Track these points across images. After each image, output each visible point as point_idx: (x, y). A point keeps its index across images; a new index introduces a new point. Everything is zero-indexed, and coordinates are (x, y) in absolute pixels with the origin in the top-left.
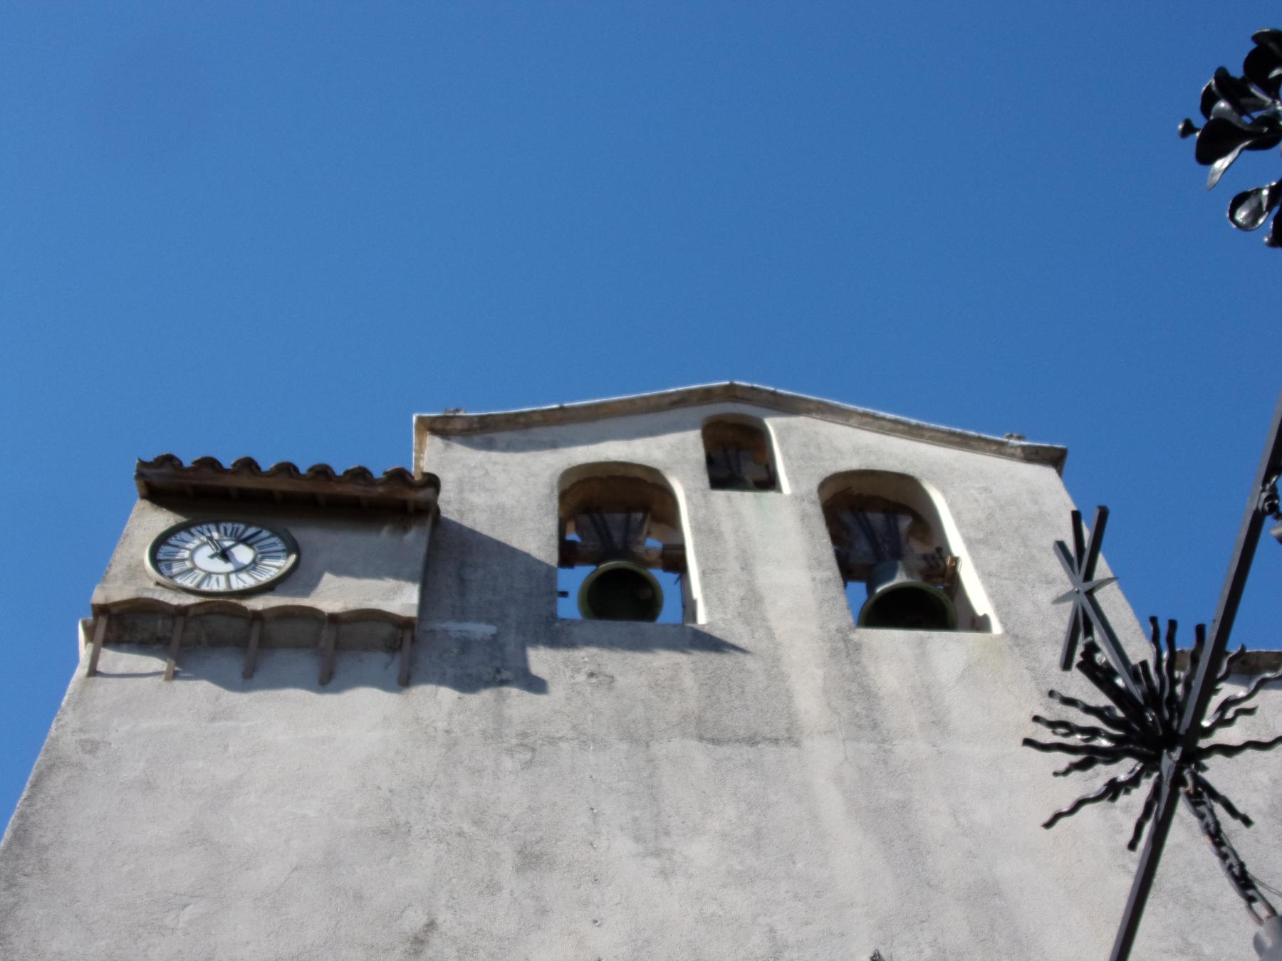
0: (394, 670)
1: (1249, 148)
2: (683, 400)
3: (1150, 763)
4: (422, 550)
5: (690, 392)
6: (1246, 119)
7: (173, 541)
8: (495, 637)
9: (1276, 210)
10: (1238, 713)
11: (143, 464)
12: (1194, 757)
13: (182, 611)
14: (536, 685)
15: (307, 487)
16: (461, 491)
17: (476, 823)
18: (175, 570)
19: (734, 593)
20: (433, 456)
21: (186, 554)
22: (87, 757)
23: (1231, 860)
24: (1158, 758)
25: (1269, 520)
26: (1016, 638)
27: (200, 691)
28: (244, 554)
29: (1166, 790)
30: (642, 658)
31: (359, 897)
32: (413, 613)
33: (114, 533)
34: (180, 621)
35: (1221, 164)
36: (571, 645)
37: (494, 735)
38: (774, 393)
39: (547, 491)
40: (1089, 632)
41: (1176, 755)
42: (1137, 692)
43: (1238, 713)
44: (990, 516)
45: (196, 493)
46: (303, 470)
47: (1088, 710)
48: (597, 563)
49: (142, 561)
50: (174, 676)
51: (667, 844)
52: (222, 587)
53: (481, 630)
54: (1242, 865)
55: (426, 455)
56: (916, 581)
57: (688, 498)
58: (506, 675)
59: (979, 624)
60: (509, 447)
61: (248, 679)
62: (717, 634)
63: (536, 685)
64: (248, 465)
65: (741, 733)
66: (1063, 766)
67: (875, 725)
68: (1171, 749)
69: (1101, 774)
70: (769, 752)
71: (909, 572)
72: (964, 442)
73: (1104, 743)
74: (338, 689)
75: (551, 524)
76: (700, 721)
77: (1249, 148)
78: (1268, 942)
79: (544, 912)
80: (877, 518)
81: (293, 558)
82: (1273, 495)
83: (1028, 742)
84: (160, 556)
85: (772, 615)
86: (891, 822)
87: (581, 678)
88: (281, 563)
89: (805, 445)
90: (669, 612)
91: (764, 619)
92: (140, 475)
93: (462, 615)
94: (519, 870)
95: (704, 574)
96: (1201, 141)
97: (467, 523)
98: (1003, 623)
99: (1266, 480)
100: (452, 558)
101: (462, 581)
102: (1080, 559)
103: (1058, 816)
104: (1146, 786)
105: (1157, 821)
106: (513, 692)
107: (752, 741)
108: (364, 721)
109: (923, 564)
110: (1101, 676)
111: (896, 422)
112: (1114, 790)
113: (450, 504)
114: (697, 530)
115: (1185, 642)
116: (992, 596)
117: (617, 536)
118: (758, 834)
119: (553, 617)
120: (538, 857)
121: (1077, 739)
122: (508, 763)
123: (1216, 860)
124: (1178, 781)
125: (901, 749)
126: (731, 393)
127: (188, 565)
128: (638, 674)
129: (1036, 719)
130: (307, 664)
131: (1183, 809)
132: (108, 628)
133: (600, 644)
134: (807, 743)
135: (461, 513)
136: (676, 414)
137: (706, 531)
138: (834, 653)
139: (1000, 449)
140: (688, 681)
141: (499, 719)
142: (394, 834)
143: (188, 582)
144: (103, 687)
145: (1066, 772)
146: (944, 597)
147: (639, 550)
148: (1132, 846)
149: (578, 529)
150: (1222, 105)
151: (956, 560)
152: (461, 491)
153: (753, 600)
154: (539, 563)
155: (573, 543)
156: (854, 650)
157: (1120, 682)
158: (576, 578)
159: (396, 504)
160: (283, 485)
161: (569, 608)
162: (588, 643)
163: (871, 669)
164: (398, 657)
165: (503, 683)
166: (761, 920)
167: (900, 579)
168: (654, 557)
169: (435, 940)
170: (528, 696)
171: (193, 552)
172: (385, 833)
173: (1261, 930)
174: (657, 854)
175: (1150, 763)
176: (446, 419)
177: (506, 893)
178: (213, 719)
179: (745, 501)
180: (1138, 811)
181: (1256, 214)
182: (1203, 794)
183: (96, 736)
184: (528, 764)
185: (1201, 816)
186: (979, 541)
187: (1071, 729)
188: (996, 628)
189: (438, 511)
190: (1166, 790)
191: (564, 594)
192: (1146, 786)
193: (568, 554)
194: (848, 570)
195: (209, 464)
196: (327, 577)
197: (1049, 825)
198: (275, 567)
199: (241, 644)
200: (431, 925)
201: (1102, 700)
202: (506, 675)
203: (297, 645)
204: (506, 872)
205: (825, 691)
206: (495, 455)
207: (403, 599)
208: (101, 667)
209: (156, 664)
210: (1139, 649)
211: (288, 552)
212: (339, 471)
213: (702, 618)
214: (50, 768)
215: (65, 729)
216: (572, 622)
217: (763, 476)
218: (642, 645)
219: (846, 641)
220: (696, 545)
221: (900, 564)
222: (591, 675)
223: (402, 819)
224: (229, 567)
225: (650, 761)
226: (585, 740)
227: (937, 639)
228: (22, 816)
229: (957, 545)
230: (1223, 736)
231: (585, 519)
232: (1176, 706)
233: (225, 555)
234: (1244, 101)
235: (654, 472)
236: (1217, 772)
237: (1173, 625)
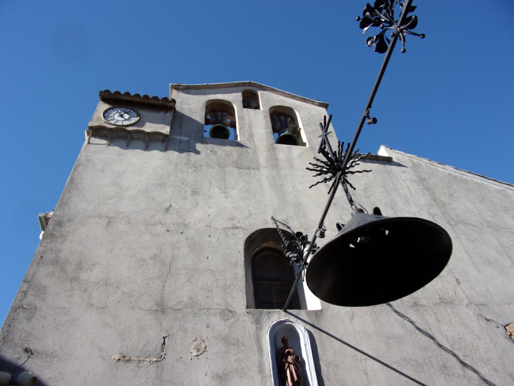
0: (163, 147)
1: (372, 25)
2: (238, 85)
3: (334, 175)
4: (171, 118)
5: (240, 83)
6: (373, 18)
7: (109, 112)
8: (188, 140)
9: (378, 41)
10: (356, 164)
11: (101, 92)
12: (344, 173)
13: (111, 129)
14: (198, 153)
15: (142, 100)
16: (181, 104)
17: (182, 183)
18: (109, 119)
19: (247, 134)
20: (174, 95)
21: (112, 115)
22: (88, 163)
23: (349, 196)
24: (336, 173)
25: (367, 119)
26: (311, 148)
27: (115, 149)
28: (126, 116)
29: (337, 181)
30: (224, 148)
31: (153, 199)
32: (168, 133)
33: (94, 109)
34: (110, 132)
35: (366, 29)
36: (207, 143)
37: (187, 164)
38: (260, 85)
39: (202, 105)
40: (325, 144)
41: (340, 173)
42: (333, 158)
43: (356, 164)
44: (309, 119)
45: (115, 100)
46: (142, 96)
47: (322, 162)
48: (214, 124)
49: (101, 117)
50: (109, 145)
51: (227, 191)
52: (121, 124)
53: (185, 139)
54: (351, 198)
55: (173, 94)
56: (290, 133)
57: (237, 110)
58: (190, 150)
59: (304, 144)
60: (194, 94)
61: (127, 146)
62: (242, 143)
63: (198, 153)
64: (128, 94)
65: (246, 167)
66: (315, 175)
67: (277, 166)
68: (339, 171)
69: (324, 176)
70: (252, 171)
71: (289, 131)
72: (305, 101)
73: (325, 170)
74: (149, 150)
75: (203, 114)
76: (236, 163)
77: (372, 25)
78: (354, 214)
79: (197, 204)
80: (283, 118)
81: (139, 118)
82: (368, 113)
83: (307, 168)
84: (106, 115)
85: (255, 139)
86: (279, 189)
87: (209, 151)
88: (136, 119)
89: (267, 99)
90: (231, 137)
91: (254, 140)
92: (100, 95)
93: (180, 135)
94: (192, 195)
95: (240, 129)
96: (361, 22)
97: (182, 112)
98: (309, 145)
99: (367, 109)
100: (178, 120)
101: (181, 126)
102: (325, 127)
103: (312, 186)
104: (333, 179)
105: (335, 187)
106: (192, 154)
107: (248, 169)
108: (155, 158)
109: (292, 130)
110: (326, 154)
111: (289, 94)
112: (326, 180)
113: (178, 107)
114: (239, 118)
115: (345, 147)
116: (307, 138)
117: (219, 118)
118: (248, 189)
119: (203, 137)
120: (197, 192)
121: (319, 169)
122: (190, 170)
123: (346, 196)
124: (340, 179)
125: (283, 172)
126: (250, 84)
127: (113, 118)
128: (224, 151)
129: (310, 163)
130: (142, 144)
131: (340, 185)
132: (93, 132)
133: (213, 144)
134: (261, 170)
135: (181, 110)
136: (235, 89)
137: (241, 118)
138: (269, 149)
139: (313, 103)
140: (234, 154)
141: (189, 160)
142: (162, 185)
143: (113, 122)
144: (91, 147)
145: (315, 176)
146: (296, 137)
147: (225, 122)
148: (329, 193)
149: (210, 116)
150: (368, 13)
151: (300, 129)
152: (181, 104)
153: (251, 136)
154: (200, 123)
155: (209, 119)
156: (274, 149)
157: (330, 156)
158: (209, 128)
159: (164, 106)
160: (136, 99)
161: (207, 135)
162: (211, 143)
163: (278, 153)
164: (164, 144)
165: (190, 151)
166: (248, 208)
167: (287, 133)
168: (228, 124)
169: (171, 209)
170: (196, 155)
171: (114, 115)
172: (160, 185)
173: (353, 211)
174: (225, 193)
175: (334, 175)
176: (178, 86)
177: (188, 199)
178: (119, 156)
179: (251, 111)
180: (330, 186)
181: (372, 43)
182: (345, 182)
183: (90, 158)
184: (195, 171)
185: (344, 187)
186: (307, 125)
187: (318, 166)
188: (308, 145)
189: (175, 109)
190: (337, 181)
191: (206, 131)
192: (333, 179)
193: (207, 122)
194: (274, 130)
195: (118, 93)
196: (147, 123)
197: (310, 187)
198: (134, 120)
199: (126, 138)
200: (170, 206)
201: (325, 159)
202: (190, 150)
203: (139, 139)
204: (188, 195)
205: (266, 158)
206: (190, 96)
207: (166, 130)
208: (91, 142)
209: (105, 142)
210: (335, 148)
211: (138, 116)
212: (151, 97)
213: (239, 139)
214: (78, 165)
215: (82, 156)
216: (207, 138)
217: (256, 106)
218: (224, 145)
219: (272, 146)
220: (238, 122)
221: (287, 129)
222: (211, 151)
223: (164, 182)
224: (123, 119)
225: (224, 172)
226: (209, 166)
227: (294, 147)
228: (72, 176)
229: (301, 125)
230: (351, 169)
231: (212, 113)
232: (342, 162)
233: (122, 116)
234: (373, 13)
235: (229, 103)
236: (350, 178)
237: (343, 143)
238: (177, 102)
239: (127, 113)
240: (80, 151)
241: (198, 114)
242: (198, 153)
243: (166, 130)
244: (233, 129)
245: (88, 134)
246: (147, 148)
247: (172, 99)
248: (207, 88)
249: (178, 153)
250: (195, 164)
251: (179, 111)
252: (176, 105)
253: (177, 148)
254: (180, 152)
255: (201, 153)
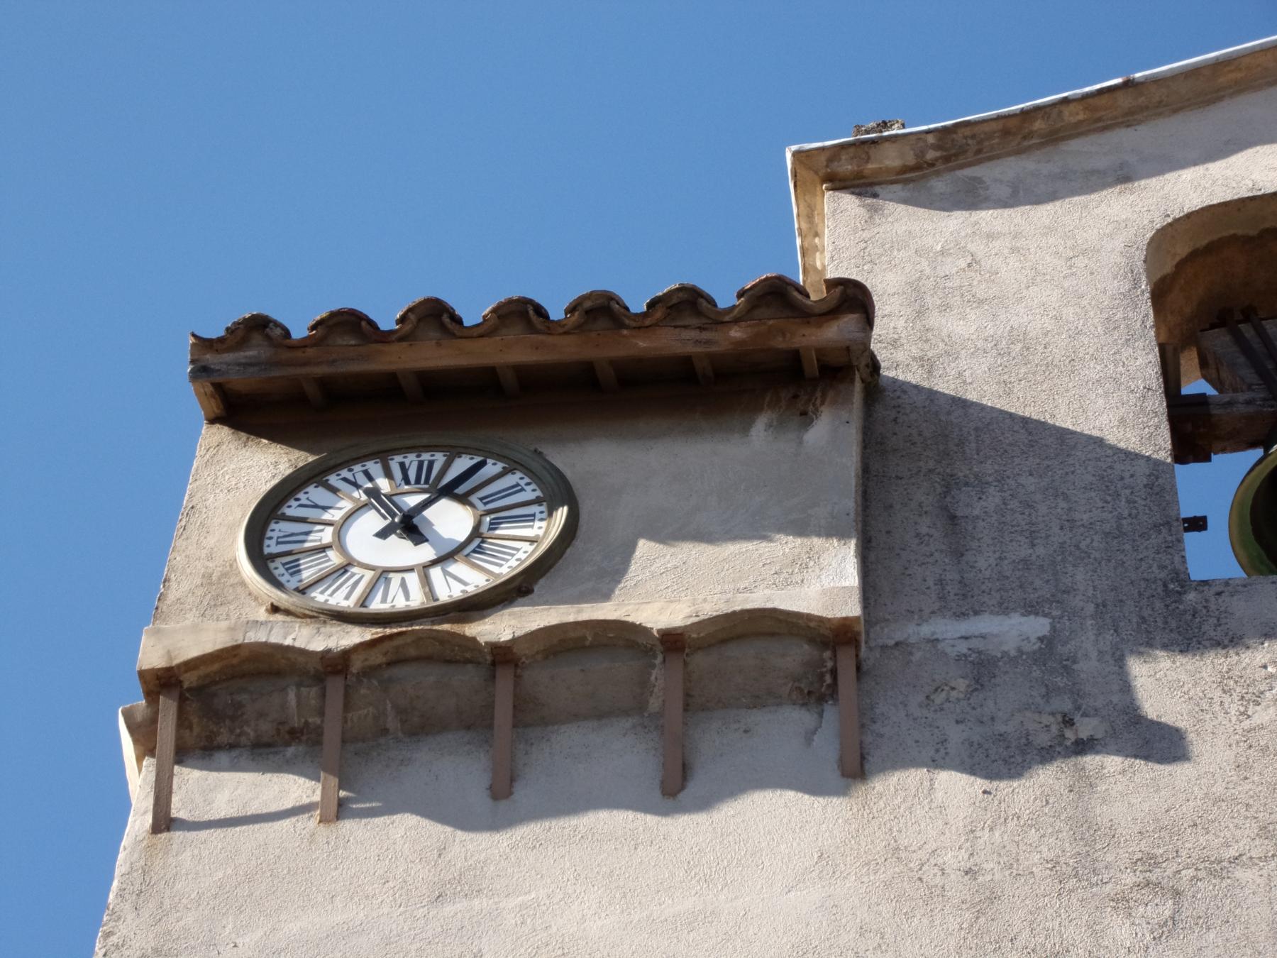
0: (827, 745)
4: (851, 460)
7: (292, 509)
8: (1048, 642)
11: (203, 344)
13: (334, 665)
15: (568, 350)
18: (307, 575)
20: (843, 239)
27: (399, 841)
28: (453, 521)
32: (852, 608)
33: (161, 507)
34: (335, 687)
36: (1231, 640)
37: (1079, 870)
45: (327, 394)
50: (341, 811)
52: (417, 600)
53: (1015, 630)
58: (1086, 728)
60: (1020, 195)
61: (504, 798)
64: (433, 316)
74: (705, 803)
81: (562, 513)
84: (271, 547)
88: (536, 529)
92: (200, 372)
93: (964, 601)
97: (946, 386)
106: (1110, 766)
113: (898, 347)
127: (334, 558)
130: (626, 750)
132: (182, 721)
141: (1087, 832)
143: (340, 598)
155: (1200, 400)
159: (777, 362)
160: (516, 351)
161: (1213, 556)
165: (1083, 747)
170: (1145, 770)
171: (341, 528)
176: (862, 148)
189: (875, 366)
191: (1197, 524)
193: (1193, 431)
195: (347, 324)
196: (644, 547)
199: (476, 723)
202: (1086, 728)
207: (822, 578)
208: (178, 809)
209: (296, 788)
212: (637, 305)
224: (426, 553)
231: (1219, 341)
233: (410, 527)
238: (883, 307)
239: (449, 491)
240: (105, 906)
241: (1093, 371)
242: (1162, 744)
243: (827, 581)
244: (354, 657)
245: (146, 746)
246: (677, 784)
247: (833, 284)
248: (1129, 119)
249: (980, 784)
250: (1151, 861)
251: (913, 376)
252: (880, 328)
253: (956, 735)
254: (991, 775)
255: (1197, 746)
